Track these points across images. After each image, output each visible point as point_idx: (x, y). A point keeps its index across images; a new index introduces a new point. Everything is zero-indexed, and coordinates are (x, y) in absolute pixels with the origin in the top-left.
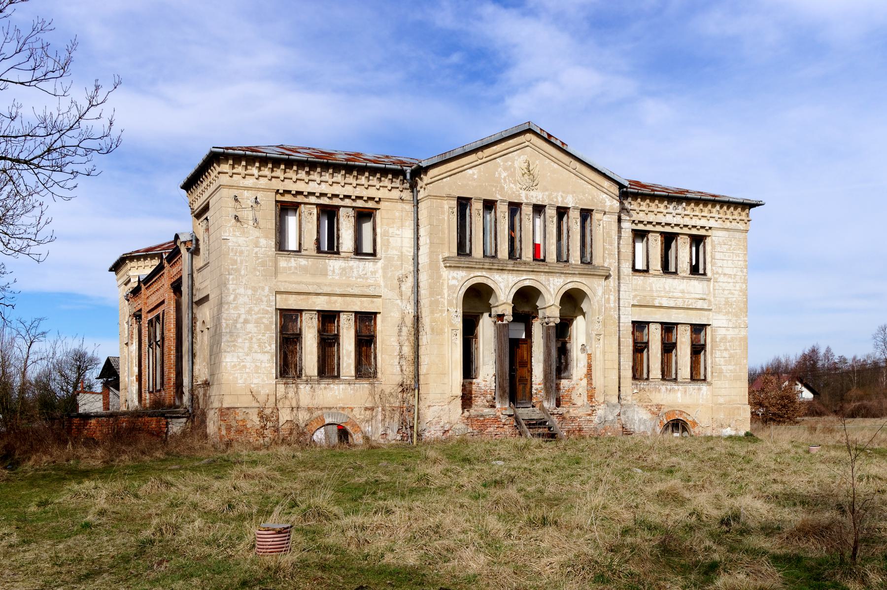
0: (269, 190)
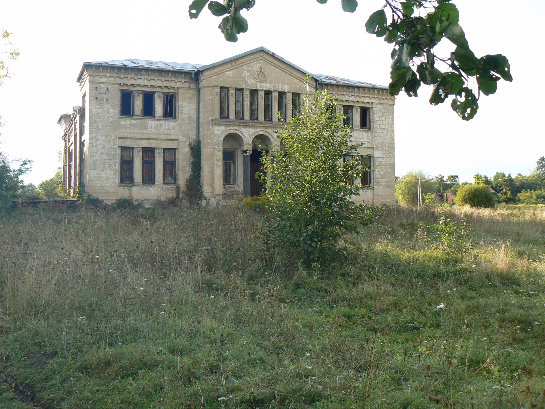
0: (115, 84)
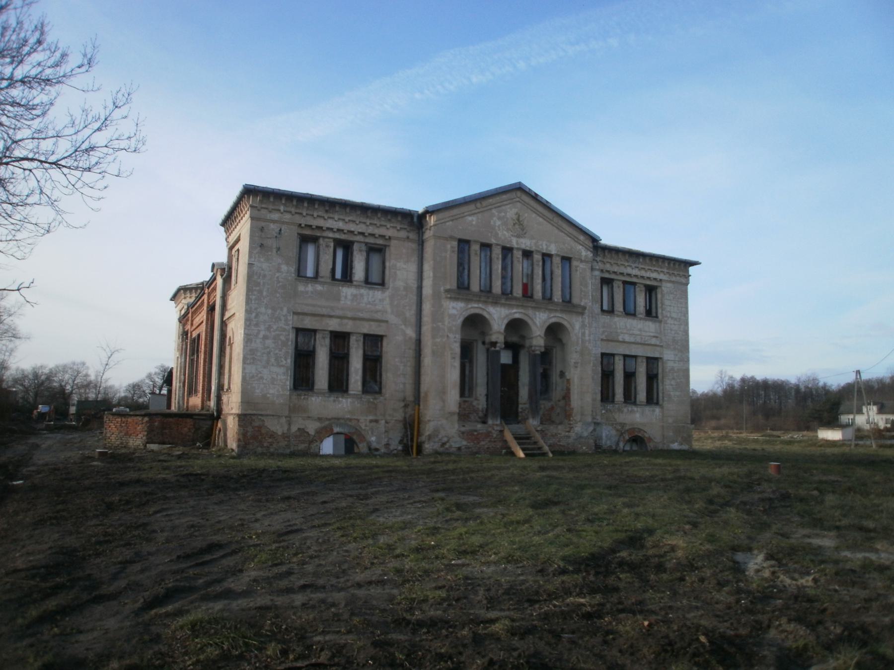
0: (293, 224)
